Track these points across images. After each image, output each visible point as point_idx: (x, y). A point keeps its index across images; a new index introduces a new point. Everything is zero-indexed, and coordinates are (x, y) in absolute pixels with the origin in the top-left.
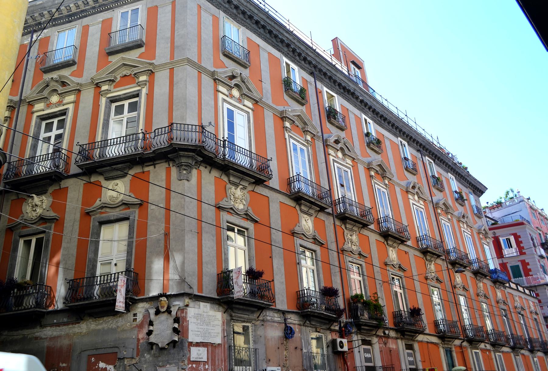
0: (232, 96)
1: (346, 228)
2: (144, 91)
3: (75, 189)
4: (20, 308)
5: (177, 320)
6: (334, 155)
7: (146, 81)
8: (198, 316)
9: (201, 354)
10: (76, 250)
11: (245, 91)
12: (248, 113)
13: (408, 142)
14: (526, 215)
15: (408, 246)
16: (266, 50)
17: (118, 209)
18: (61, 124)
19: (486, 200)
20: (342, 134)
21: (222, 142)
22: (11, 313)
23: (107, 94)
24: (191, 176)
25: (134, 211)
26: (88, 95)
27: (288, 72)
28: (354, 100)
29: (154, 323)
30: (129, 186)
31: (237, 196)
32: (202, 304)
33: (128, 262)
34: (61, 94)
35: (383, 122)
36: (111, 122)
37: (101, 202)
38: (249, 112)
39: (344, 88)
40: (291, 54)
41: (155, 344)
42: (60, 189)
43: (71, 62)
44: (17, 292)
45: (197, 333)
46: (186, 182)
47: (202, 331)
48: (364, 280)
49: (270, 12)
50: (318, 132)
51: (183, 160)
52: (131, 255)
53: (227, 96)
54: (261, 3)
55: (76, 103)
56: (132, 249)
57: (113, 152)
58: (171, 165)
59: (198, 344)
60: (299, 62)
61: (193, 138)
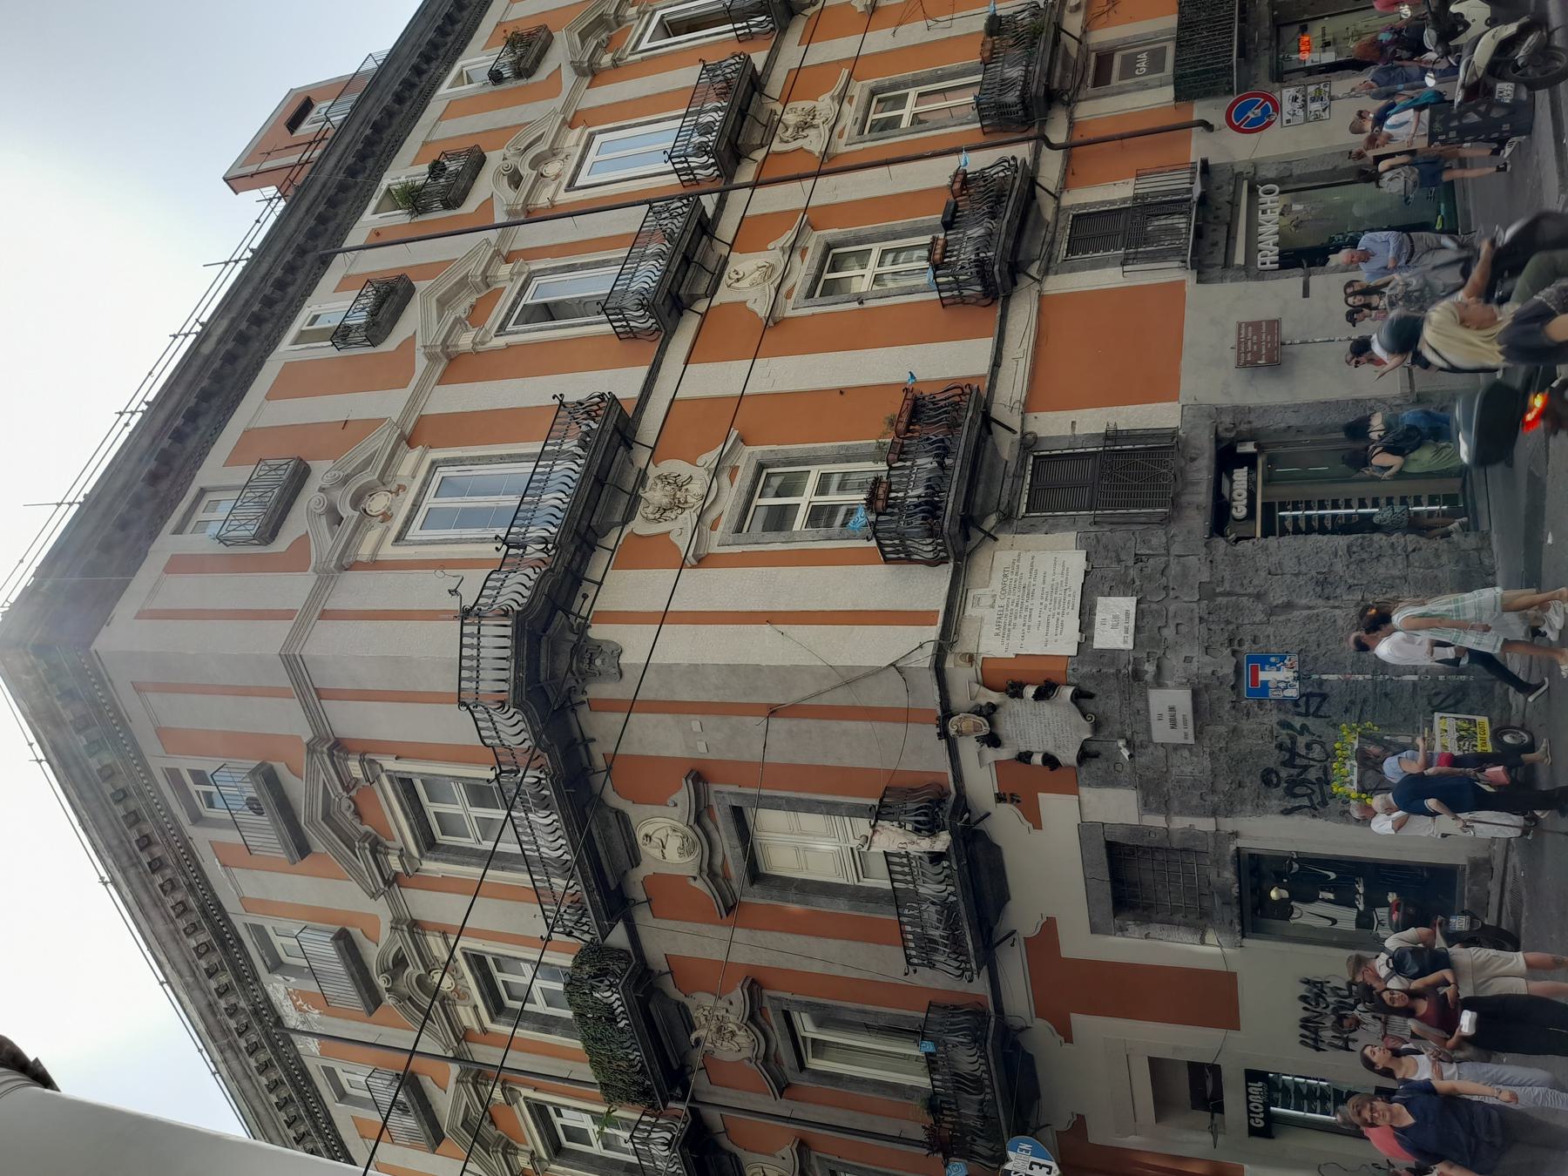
0: (386, 517)
2: (390, 764)
5: (1015, 690)
7: (361, 761)
8: (1004, 630)
9: (1115, 617)
10: (831, 941)
11: (370, 476)
16: (259, 409)
17: (715, 835)
20: (494, 159)
21: (512, 551)
22: (999, 1104)
23: (411, 856)
24: (608, 642)
27: (318, 335)
28: (396, 121)
29: (1023, 749)
30: (648, 807)
31: (665, 501)
32: (971, 611)
33: (855, 812)
34: (425, 966)
35: (458, 27)
39: (362, 157)
40: (267, 327)
42: (671, 972)
43: (341, 943)
45: (1052, 629)
47: (1047, 612)
48: (916, 83)
49: (150, 398)
50: (488, 241)
53: (388, 529)
54: (127, 425)
56: (819, 802)
58: (584, 698)
60: (292, 300)
61: (495, 638)
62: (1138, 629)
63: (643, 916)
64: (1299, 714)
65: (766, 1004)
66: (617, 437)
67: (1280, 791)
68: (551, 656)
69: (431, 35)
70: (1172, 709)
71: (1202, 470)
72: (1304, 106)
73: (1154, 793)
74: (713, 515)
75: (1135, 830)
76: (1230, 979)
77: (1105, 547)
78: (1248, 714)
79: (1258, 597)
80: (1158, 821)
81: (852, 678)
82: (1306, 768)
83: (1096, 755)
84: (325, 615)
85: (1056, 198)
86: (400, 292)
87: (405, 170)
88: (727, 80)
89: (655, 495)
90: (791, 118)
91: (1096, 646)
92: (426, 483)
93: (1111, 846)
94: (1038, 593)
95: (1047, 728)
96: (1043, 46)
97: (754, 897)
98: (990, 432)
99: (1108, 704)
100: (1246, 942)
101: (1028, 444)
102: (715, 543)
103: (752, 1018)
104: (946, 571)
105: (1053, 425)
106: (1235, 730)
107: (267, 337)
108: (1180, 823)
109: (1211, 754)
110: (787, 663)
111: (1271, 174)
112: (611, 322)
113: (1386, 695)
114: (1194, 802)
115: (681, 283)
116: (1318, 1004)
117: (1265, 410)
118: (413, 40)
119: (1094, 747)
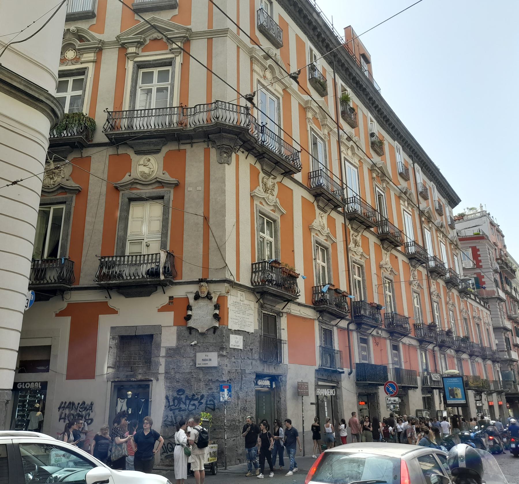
1: (352, 228)
3: (99, 161)
4: (42, 282)
5: (217, 307)
6: (346, 153)
10: (102, 226)
12: (278, 98)
13: (403, 147)
14: (486, 230)
15: (398, 251)
17: (150, 187)
18: (79, 84)
19: (457, 211)
25: (165, 192)
26: (110, 57)
29: (193, 308)
34: (79, 50)
36: (139, 91)
37: (131, 178)
38: (279, 98)
41: (193, 328)
43: (91, 14)
44: (41, 265)
45: (235, 321)
46: (226, 165)
48: (363, 280)
51: (226, 142)
52: (167, 237)
55: (97, 62)
56: (167, 230)
57: (139, 124)
58: (210, 147)
59: (237, 332)
62: (234, 349)
63: (111, 151)
64: (207, 402)
65: (68, 195)
66: (288, 170)
67: (175, 394)
68: (229, 138)
69: (385, 113)
70: (210, 360)
71: (272, 371)
72: (392, 404)
73: (172, 352)
74: (264, 203)
75: (158, 346)
76: (93, 377)
77: (254, 339)
78: (206, 385)
79: (241, 388)
80: (163, 352)
81: (221, 250)
82: (185, 404)
83: (190, 333)
84: (238, 48)
85: (336, 325)
86: (323, 92)
87: (354, 101)
88: (369, 217)
89: (270, 182)
90: (358, 238)
91: (231, 335)
92: (273, 94)
93: (151, 336)
94: (244, 316)
95: (202, 316)
96: (373, 323)
97: (122, 198)
98: (285, 301)
99: (211, 339)
100: (110, 383)
101: (279, 314)
102: (256, 202)
103: (62, 188)
104: (249, 285)
105: (283, 322)
106: (200, 380)
107: (313, 38)
108: (162, 361)
109: (191, 372)
110: (226, 227)
111: (338, 393)
112: (313, 172)
113: (215, 430)
114: (171, 366)
115: (325, 197)
116: (81, 408)
117: (285, 391)
118: (385, 107)
119: (194, 332)
